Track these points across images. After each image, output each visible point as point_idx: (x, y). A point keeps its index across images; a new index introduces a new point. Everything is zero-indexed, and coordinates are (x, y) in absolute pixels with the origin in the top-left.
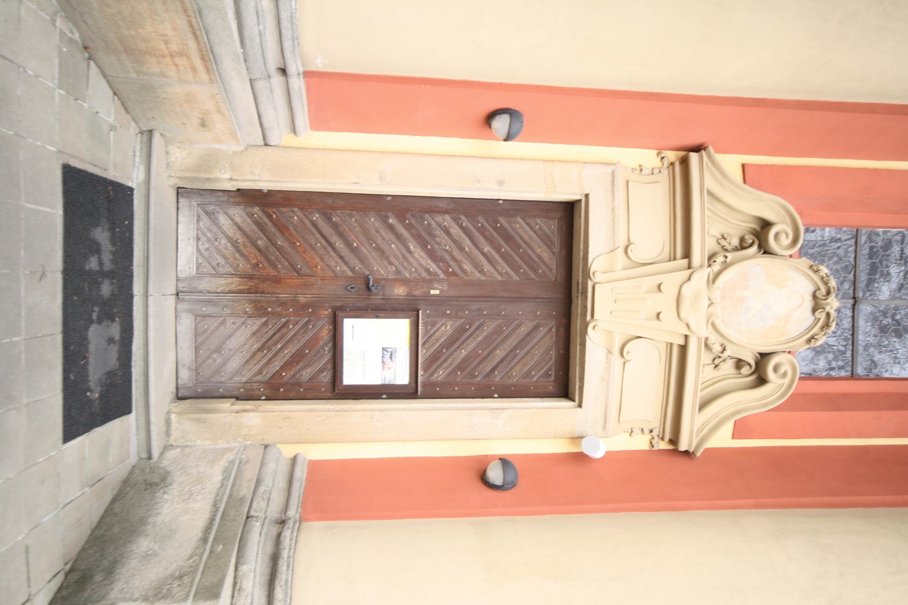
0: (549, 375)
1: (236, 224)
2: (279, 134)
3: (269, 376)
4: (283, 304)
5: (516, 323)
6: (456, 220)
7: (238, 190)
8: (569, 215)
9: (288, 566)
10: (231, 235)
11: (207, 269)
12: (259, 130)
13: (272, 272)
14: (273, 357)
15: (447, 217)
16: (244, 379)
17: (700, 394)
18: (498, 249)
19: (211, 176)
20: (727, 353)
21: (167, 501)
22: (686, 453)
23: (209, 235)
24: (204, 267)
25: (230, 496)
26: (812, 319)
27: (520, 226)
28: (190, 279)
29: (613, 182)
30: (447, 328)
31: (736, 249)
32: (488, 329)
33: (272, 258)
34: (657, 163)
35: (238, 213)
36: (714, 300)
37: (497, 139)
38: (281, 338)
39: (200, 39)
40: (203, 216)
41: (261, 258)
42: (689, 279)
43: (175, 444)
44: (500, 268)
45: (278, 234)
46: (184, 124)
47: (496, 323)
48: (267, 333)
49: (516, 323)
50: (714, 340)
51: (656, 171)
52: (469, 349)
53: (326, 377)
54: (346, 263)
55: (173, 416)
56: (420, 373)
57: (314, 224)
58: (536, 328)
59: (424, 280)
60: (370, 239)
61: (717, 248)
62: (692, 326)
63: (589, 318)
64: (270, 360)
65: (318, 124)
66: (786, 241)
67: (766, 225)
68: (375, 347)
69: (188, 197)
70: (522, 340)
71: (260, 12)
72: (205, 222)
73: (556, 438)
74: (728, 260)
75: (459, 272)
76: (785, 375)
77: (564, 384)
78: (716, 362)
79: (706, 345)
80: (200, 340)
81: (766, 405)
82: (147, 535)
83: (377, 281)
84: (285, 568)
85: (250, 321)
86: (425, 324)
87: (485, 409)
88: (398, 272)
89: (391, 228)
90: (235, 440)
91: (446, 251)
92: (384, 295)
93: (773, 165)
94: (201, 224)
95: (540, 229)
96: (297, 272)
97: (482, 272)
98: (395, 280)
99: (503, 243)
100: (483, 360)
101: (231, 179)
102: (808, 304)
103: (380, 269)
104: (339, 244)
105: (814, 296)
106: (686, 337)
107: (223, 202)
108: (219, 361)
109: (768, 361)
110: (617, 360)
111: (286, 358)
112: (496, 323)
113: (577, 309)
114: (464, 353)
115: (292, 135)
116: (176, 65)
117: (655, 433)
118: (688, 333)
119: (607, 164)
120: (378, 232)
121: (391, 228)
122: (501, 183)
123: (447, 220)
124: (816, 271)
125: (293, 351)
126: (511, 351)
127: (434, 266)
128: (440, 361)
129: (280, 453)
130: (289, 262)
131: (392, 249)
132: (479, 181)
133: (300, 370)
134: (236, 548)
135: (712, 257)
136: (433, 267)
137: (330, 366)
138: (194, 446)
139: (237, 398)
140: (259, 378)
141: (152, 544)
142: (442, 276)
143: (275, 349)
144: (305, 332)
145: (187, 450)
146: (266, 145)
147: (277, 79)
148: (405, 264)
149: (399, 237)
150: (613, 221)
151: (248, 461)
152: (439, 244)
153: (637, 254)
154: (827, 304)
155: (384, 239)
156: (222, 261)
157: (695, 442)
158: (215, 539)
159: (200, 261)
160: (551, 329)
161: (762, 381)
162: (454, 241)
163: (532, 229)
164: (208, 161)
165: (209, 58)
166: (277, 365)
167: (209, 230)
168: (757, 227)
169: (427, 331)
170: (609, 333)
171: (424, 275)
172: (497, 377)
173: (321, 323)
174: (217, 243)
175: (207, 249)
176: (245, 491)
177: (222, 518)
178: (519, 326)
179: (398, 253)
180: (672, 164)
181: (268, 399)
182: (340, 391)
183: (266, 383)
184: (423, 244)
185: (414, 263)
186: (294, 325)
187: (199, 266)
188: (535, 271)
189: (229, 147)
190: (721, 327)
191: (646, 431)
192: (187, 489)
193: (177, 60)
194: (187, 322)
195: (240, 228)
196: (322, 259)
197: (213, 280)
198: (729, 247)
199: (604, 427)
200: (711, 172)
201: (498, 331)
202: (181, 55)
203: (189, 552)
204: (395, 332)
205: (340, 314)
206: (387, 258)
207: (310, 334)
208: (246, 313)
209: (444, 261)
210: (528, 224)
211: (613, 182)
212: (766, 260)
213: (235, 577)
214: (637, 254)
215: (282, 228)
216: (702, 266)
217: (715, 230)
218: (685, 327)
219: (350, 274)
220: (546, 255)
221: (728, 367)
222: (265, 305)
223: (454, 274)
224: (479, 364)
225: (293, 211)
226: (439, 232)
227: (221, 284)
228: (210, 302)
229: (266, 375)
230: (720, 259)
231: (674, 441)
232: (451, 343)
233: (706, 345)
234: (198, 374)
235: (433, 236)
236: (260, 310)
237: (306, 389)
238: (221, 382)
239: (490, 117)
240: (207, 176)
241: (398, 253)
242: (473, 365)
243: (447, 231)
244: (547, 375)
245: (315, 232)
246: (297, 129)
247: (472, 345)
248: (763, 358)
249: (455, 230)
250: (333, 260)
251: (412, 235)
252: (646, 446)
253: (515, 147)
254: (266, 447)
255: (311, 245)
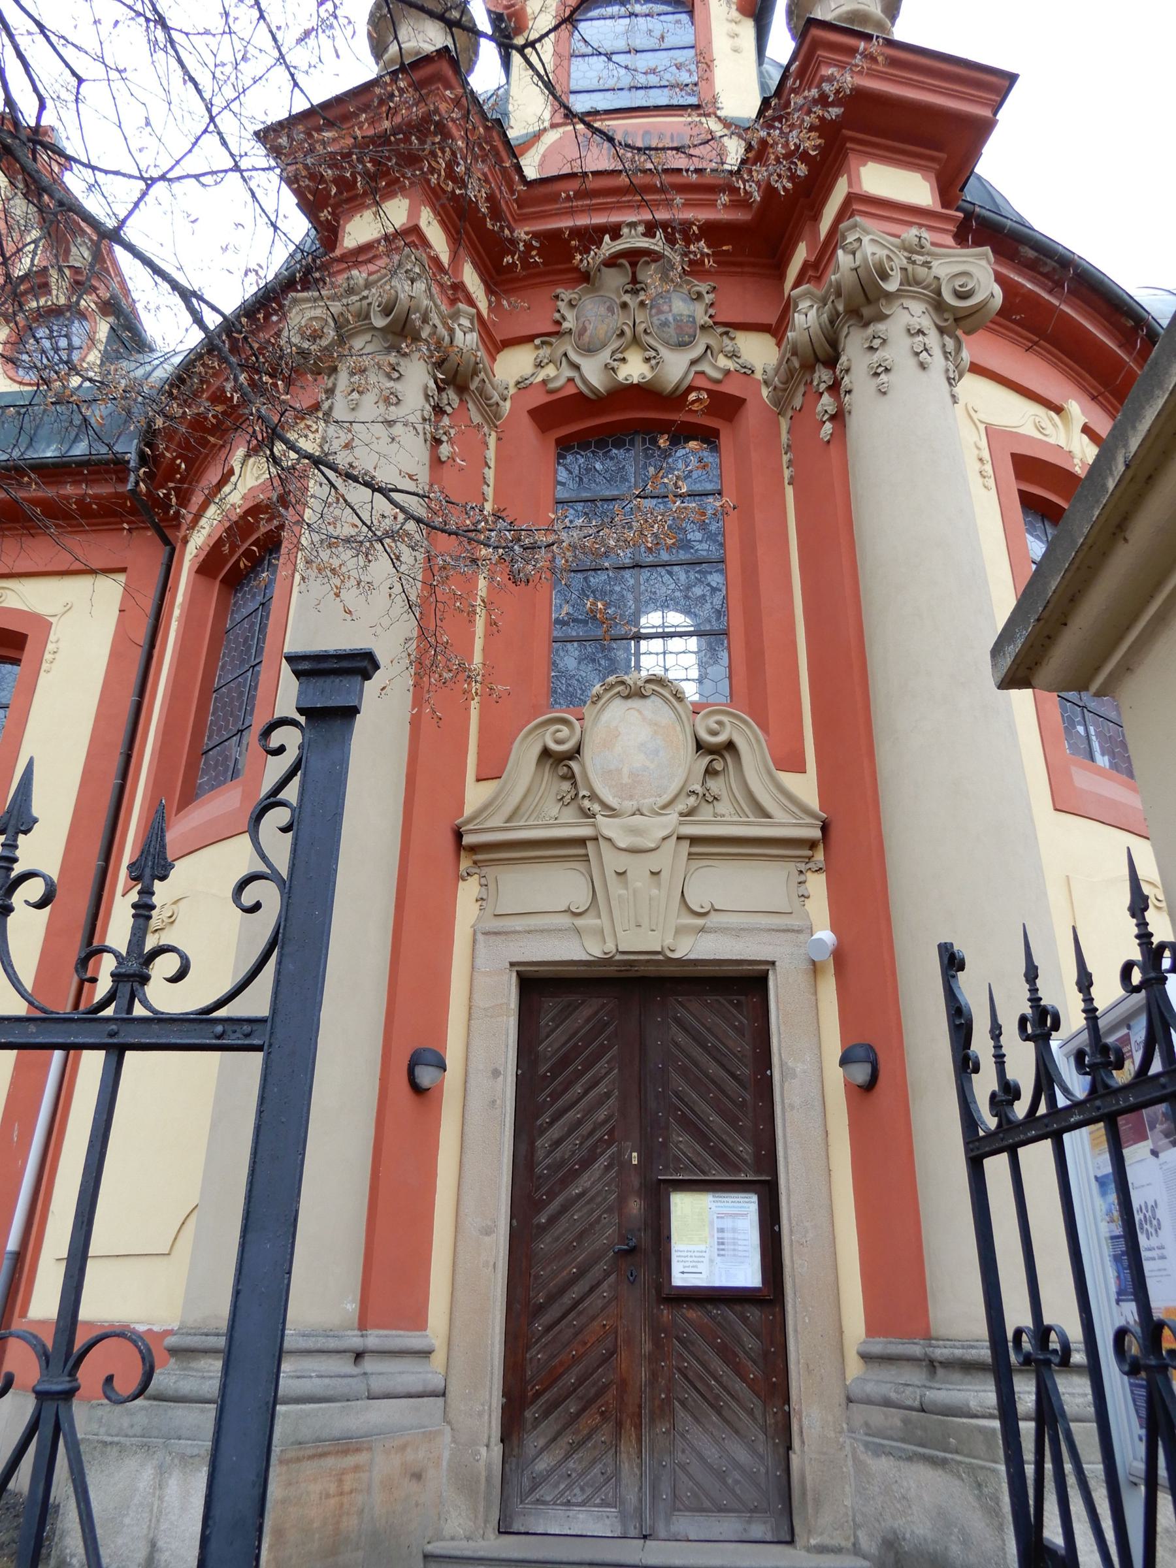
0: (739, 1003)
1: (546, 1447)
2: (431, 1373)
3: (755, 1400)
4: (654, 1376)
5: (674, 1050)
6: (542, 1131)
7: (502, 1441)
8: (538, 987)
9: (972, 1347)
10: (563, 1452)
11: (608, 1491)
12: (425, 1399)
13: (613, 1390)
14: (729, 1393)
15: (538, 1143)
16: (762, 1437)
17: (752, 819)
18: (579, 1075)
19: (484, 1474)
20: (697, 787)
21: (913, 1532)
22: (825, 828)
23: (562, 1486)
24: (606, 1495)
25: (903, 1440)
26: (653, 698)
27: (550, 1046)
28: (623, 1517)
29: (496, 933)
30: (682, 1141)
31: (575, 784)
32: (682, 1086)
33: (593, 1391)
34: (473, 882)
35: (534, 1441)
36: (635, 808)
37: (443, 1081)
38: (702, 1379)
39: (326, 1449)
40: (536, 1495)
41: (593, 1409)
42: (609, 840)
43: (852, 1539)
44: (603, 1071)
45: (560, 1383)
46: (417, 1505)
47: (673, 1075)
48: (694, 1400)
49: (674, 1050)
50: (681, 806)
51: (483, 881)
52: (708, 1110)
53: (754, 1314)
54: (599, 1284)
55: (813, 1542)
56: (742, 1177)
57: (548, 1329)
58: (679, 1022)
59: (619, 1173)
60: (568, 1250)
61: (574, 806)
62: (665, 833)
63: (661, 957)
64: (732, 1397)
65: (418, 1321)
66: (565, 731)
67: (546, 753)
68: (710, 1240)
69: (510, 1517)
70: (694, 1039)
71: (299, 1374)
72: (546, 1492)
73: (816, 993)
74: (587, 793)
75: (608, 1126)
76: (719, 723)
77: (746, 986)
78: (710, 799)
79: (689, 814)
80: (707, 1504)
81: (758, 741)
82: (946, 1548)
83: (623, 1239)
84: (974, 1351)
85: (680, 1426)
86: (677, 1171)
87: (782, 1087)
88: (609, 1210)
89: (552, 1220)
90: (842, 1448)
91: (581, 1144)
92: (639, 1230)
93: (480, 732)
94: (548, 1498)
95: (552, 1020)
96: (612, 1354)
97: (608, 1095)
98: (620, 1215)
99: (571, 1068)
100: (723, 1092)
101: (487, 1446)
102: (636, 703)
103: (607, 1236)
104: (574, 1293)
105: (628, 697)
106: (679, 838)
107: (518, 1464)
108: (737, 1475)
109: (705, 742)
110: (714, 920)
111: (730, 1372)
112: (673, 1075)
113: (651, 970)
114: (714, 1118)
115: (433, 1356)
116: (351, 1492)
117: (802, 867)
118: (674, 837)
119: (474, 941)
120: (557, 1239)
121: (552, 1220)
122: (496, 1073)
123: (543, 1143)
124: (599, 697)
125: (720, 1362)
126: (709, 1053)
127: (602, 1159)
128: (726, 1150)
129: (857, 1378)
130: (599, 1367)
131: (580, 1218)
132: (494, 1102)
133: (746, 1353)
134: (965, 1420)
135: (588, 814)
136: (603, 1161)
137: (738, 1308)
138: (853, 1508)
139: (789, 1447)
140: (758, 1413)
141: (953, 1538)
142: (614, 1149)
143: (718, 1389)
144: (693, 1344)
145: (859, 1519)
146: (444, 1395)
147: (369, 1365)
148: (599, 1199)
149: (564, 1209)
150: (542, 931)
151: (867, 1424)
152: (573, 1153)
153: (581, 900)
154: (635, 684)
155: (567, 1230)
156: (596, 1470)
157: (809, 820)
158: (945, 1451)
159: (598, 1501)
160: (680, 1003)
161: (730, 746)
162: (570, 1132)
163: (553, 1031)
164: (464, 1481)
165: (346, 1445)
166: (740, 1387)
167: (556, 1485)
168: (551, 761)
169: (686, 1168)
170: (680, 931)
171: (613, 1173)
172: (745, 1071)
173: (680, 1320)
174: (574, 1475)
175: (582, 1489)
176: (895, 1418)
177: (923, 1446)
178: (677, 1045)
179: (585, 1210)
180: (475, 863)
181: (787, 1400)
182: (770, 1296)
183: (764, 1403)
184: (574, 1175)
185: (599, 1186)
186: (685, 1360)
187: (604, 1504)
188: (606, 1025)
189: (445, 1447)
190: (666, 798)
191: (802, 878)
192: (898, 1506)
193: (347, 1488)
194: (684, 1524)
195: (554, 1439)
196: (593, 1318)
197: (624, 1482)
198: (573, 793)
199: (799, 931)
200: (486, 819)
201: (684, 1072)
202: (340, 1481)
203: (957, 1482)
204: (686, 1209)
205: (666, 1291)
206: (592, 1225)
207: (696, 1336)
208: (668, 1432)
209: (595, 1146)
210: (547, 1037)
211: (496, 933)
212: (587, 752)
213: (984, 1417)
214: (581, 900)
215: (554, 1378)
216: (594, 825)
217: (553, 809)
218: (666, 842)
219: (612, 1278)
220: (586, 1011)
221: (715, 785)
222: (657, 1403)
223: (611, 1132)
224: (728, 1097)
225: (531, 1359)
226: (557, 1154)
227: (628, 1469)
228: (654, 1487)
229: (754, 1403)
230: (586, 803)
231: (812, 844)
232: (700, 1135)
233: (689, 814)
234: (755, 1510)
235: (562, 1163)
236: (664, 1410)
237: (772, 1345)
238: (767, 1472)
239: (417, 1089)
240: (483, 1480)
241: (585, 1210)
242: (730, 1105)
243: (557, 1143)
244: (738, 1006)
245: (557, 1328)
246: (427, 1349)
247: (703, 1107)
248: (700, 746)
249: (555, 1132)
250: (594, 1303)
251: (561, 1191)
252: (822, 877)
253: (453, 1055)
254: (850, 1400)
255: (576, 1334)
